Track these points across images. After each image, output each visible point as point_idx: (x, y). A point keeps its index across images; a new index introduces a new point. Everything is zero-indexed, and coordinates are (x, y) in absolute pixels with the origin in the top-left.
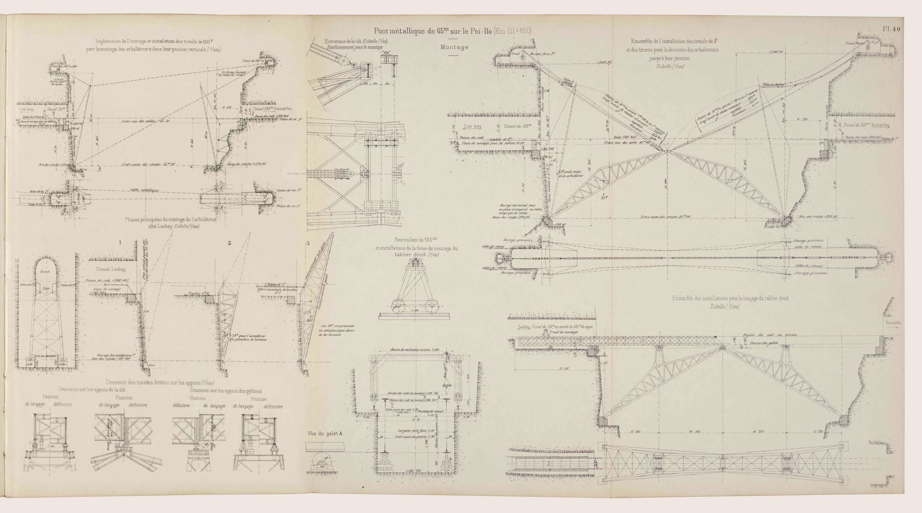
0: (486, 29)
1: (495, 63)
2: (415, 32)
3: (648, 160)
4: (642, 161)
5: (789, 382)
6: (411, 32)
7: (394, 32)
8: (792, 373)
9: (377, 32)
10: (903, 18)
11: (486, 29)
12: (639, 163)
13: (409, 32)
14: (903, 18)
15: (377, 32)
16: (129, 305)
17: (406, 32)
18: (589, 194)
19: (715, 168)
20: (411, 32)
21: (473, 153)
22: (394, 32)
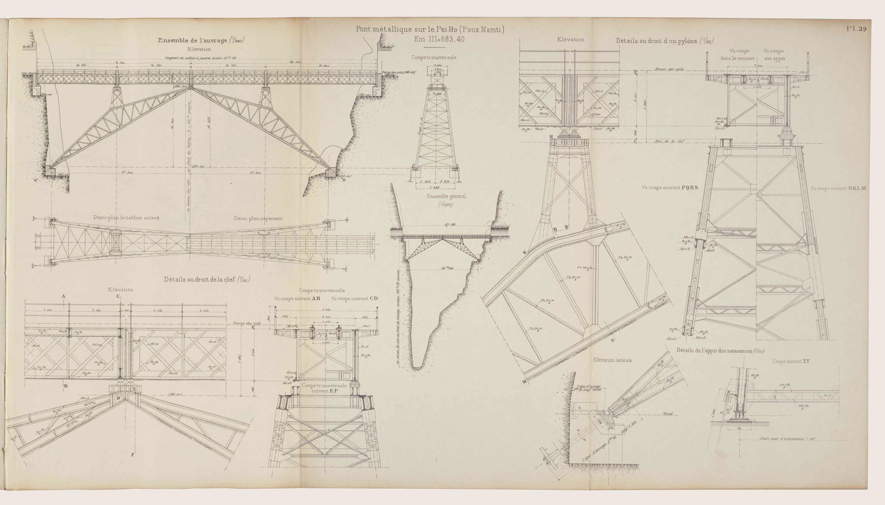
0: (451, 28)
1: (382, 89)
2: (401, 30)
3: (168, 97)
4: (161, 99)
5: (463, 250)
6: (396, 30)
7: (377, 29)
8: (464, 246)
9: (359, 30)
10: (866, 488)
11: (451, 28)
12: (310, 152)
13: (394, 30)
14: (866, 488)
15: (359, 30)
16: (430, 347)
17: (391, 30)
18: (97, 139)
19: (277, 120)
20: (396, 30)
21: (46, 141)
22: (377, 29)
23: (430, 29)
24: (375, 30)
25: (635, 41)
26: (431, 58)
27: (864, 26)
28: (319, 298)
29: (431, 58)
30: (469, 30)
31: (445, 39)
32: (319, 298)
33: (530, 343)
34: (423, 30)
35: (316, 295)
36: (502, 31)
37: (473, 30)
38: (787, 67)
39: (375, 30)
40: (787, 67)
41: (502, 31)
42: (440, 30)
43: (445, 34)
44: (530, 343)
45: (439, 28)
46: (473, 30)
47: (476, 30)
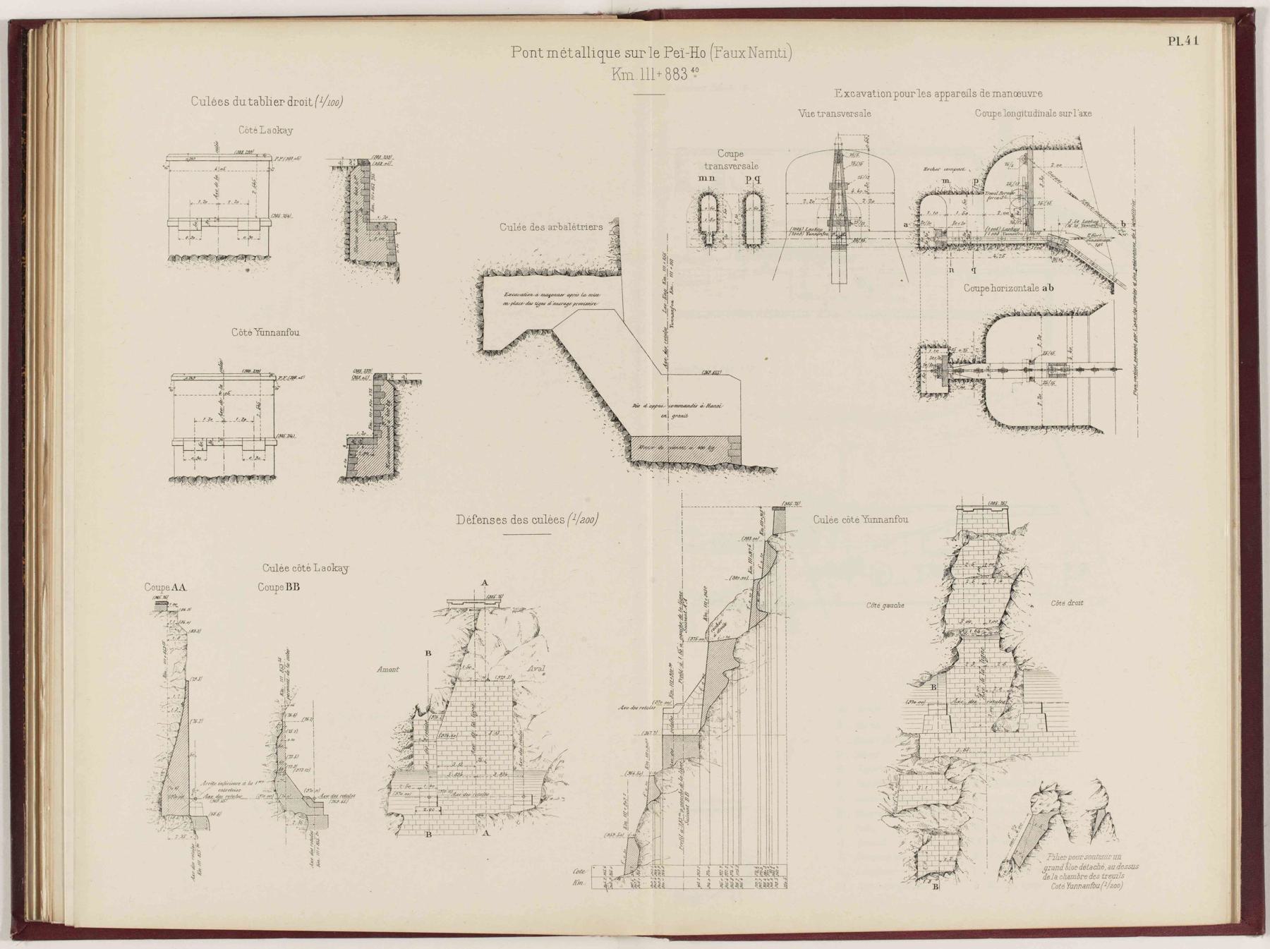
11: (695, 50)
23: (653, 53)
24: (551, 56)
25: (972, 94)
26: (825, 115)
27: (20, 31)
28: (296, 587)
29: (825, 115)
30: (727, 55)
31: (672, 73)
32: (296, 587)
33: (740, 823)
34: (639, 53)
35: (292, 577)
36: (788, 54)
37: (734, 53)
38: (185, 460)
39: (551, 56)
40: (185, 460)
41: (788, 54)
42: (671, 55)
43: (680, 63)
44: (740, 823)
45: (516, 49)
46: (734, 53)
47: (739, 54)
